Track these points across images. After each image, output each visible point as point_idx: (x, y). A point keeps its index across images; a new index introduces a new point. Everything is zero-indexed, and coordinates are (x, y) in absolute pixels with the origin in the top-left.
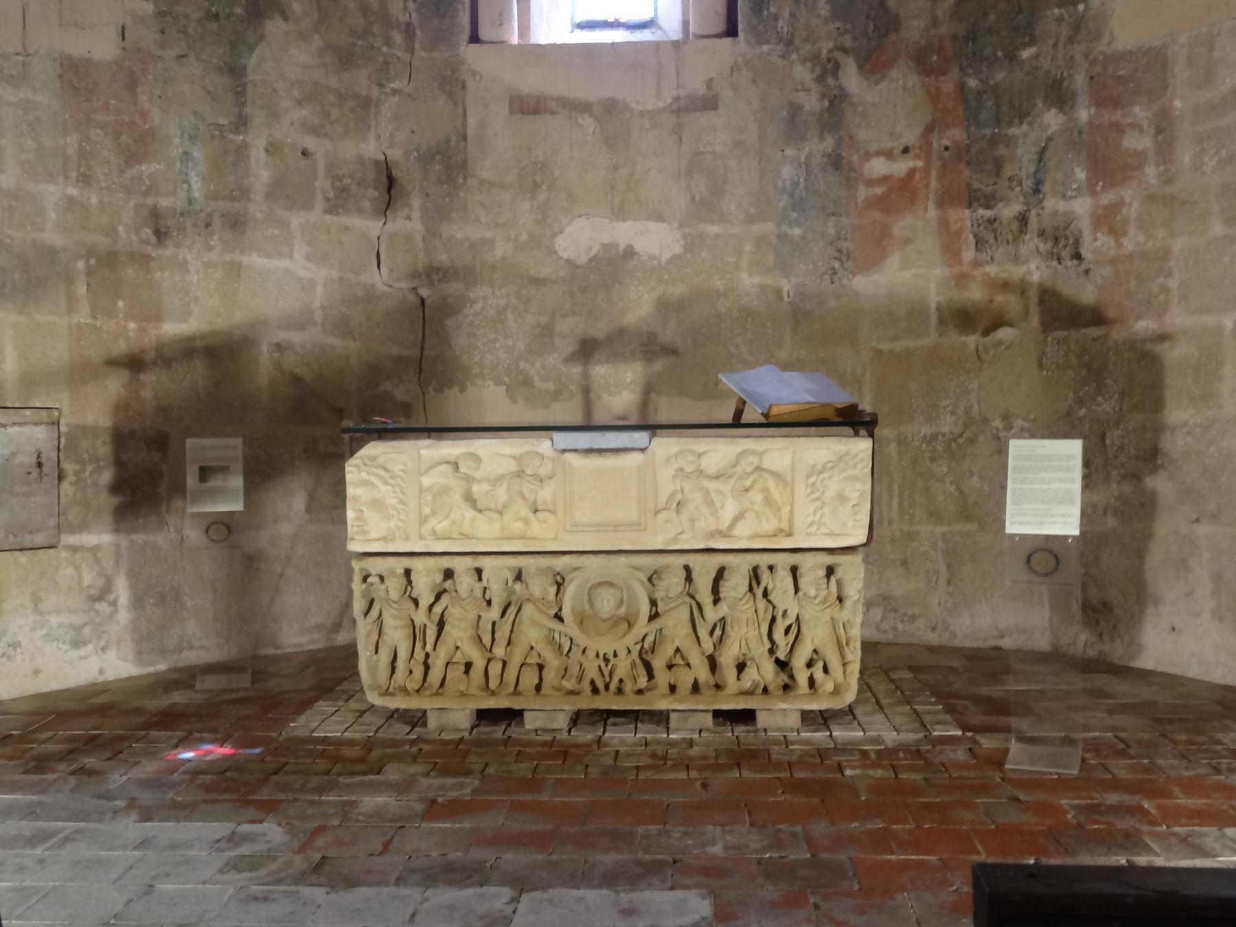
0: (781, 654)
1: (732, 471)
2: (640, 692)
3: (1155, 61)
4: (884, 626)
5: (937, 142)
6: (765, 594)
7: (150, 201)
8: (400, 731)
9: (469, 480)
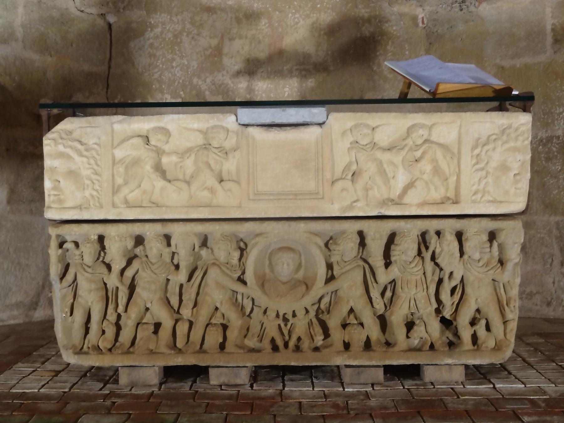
0: (447, 313)
1: (405, 143)
2: (316, 349)
6: (433, 258)
8: (94, 387)
9: (159, 152)
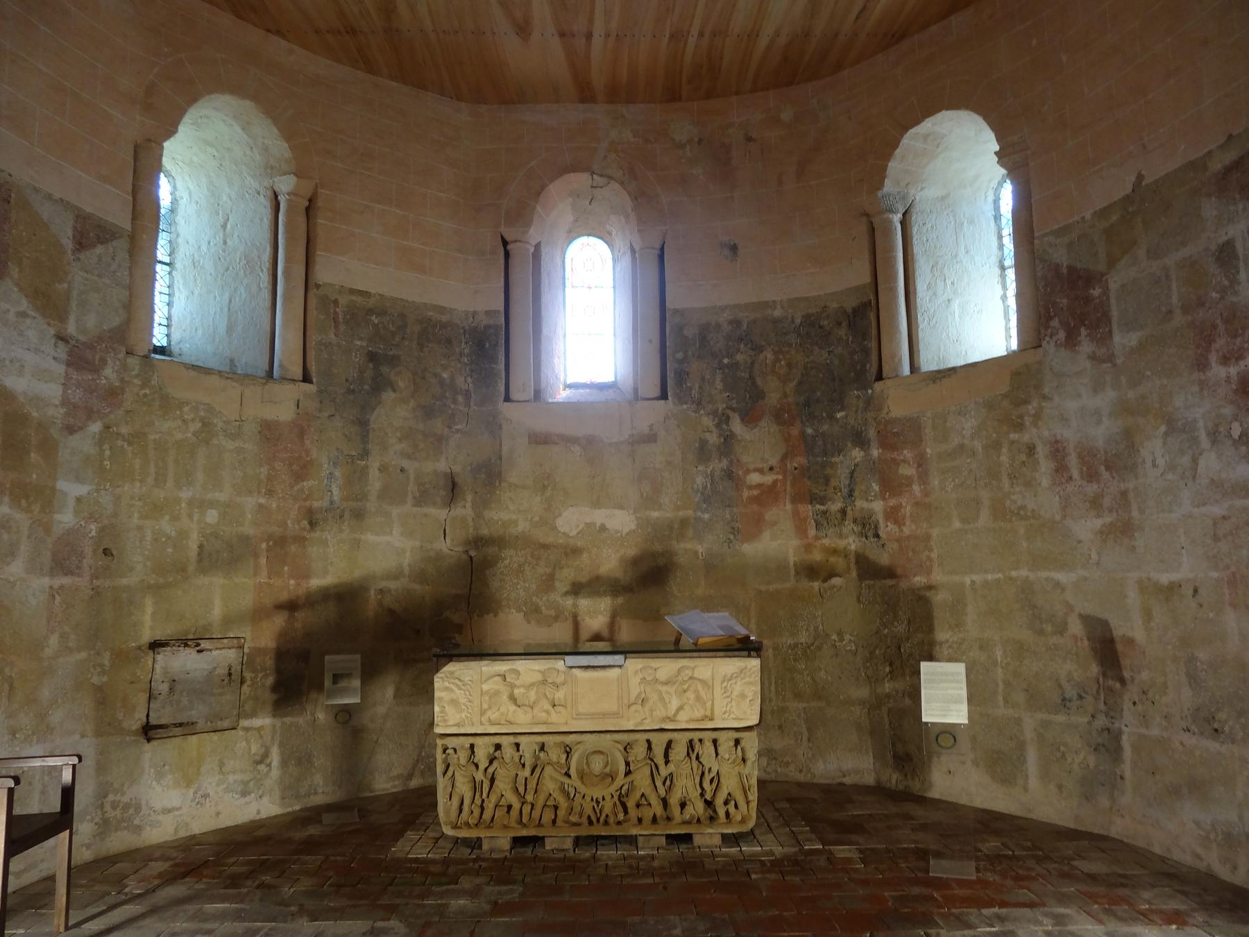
0: (708, 797)
2: (619, 823)
3: (914, 425)
4: (769, 770)
5: (790, 465)
6: (697, 758)
7: (308, 503)
9: (513, 686)
